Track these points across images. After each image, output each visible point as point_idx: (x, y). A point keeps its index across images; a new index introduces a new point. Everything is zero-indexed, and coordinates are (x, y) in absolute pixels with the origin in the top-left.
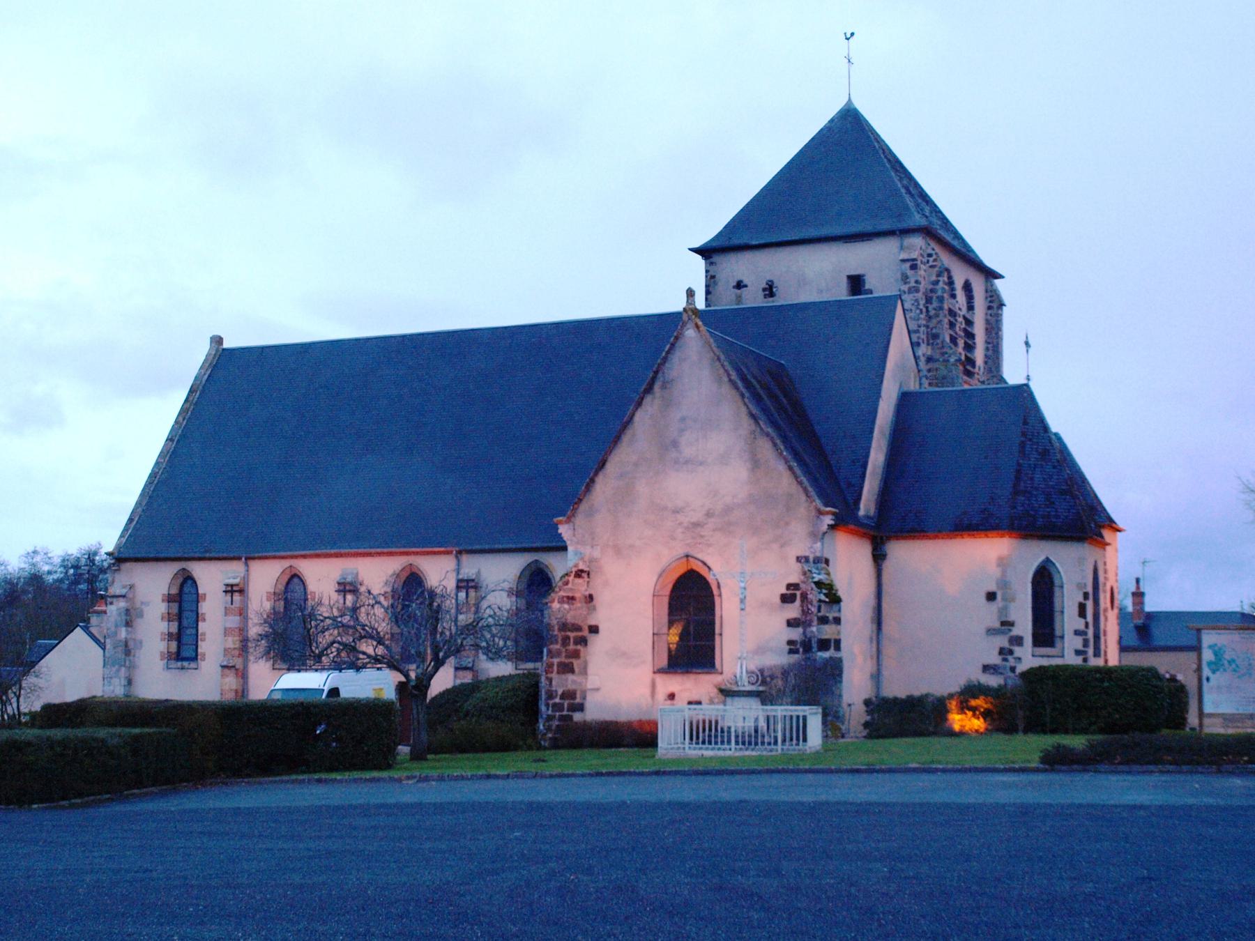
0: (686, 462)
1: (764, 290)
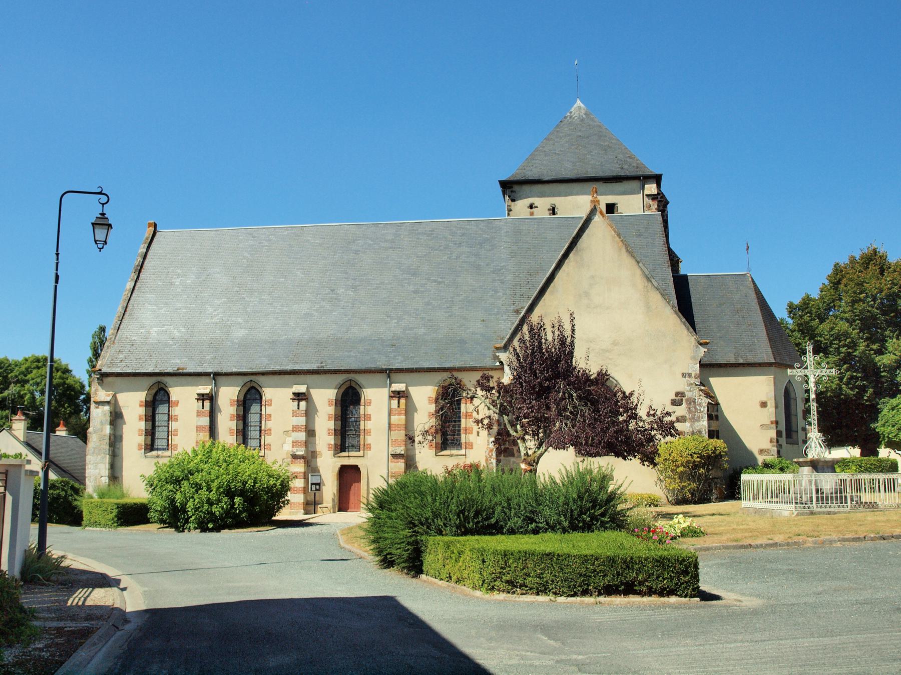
1: (549, 210)
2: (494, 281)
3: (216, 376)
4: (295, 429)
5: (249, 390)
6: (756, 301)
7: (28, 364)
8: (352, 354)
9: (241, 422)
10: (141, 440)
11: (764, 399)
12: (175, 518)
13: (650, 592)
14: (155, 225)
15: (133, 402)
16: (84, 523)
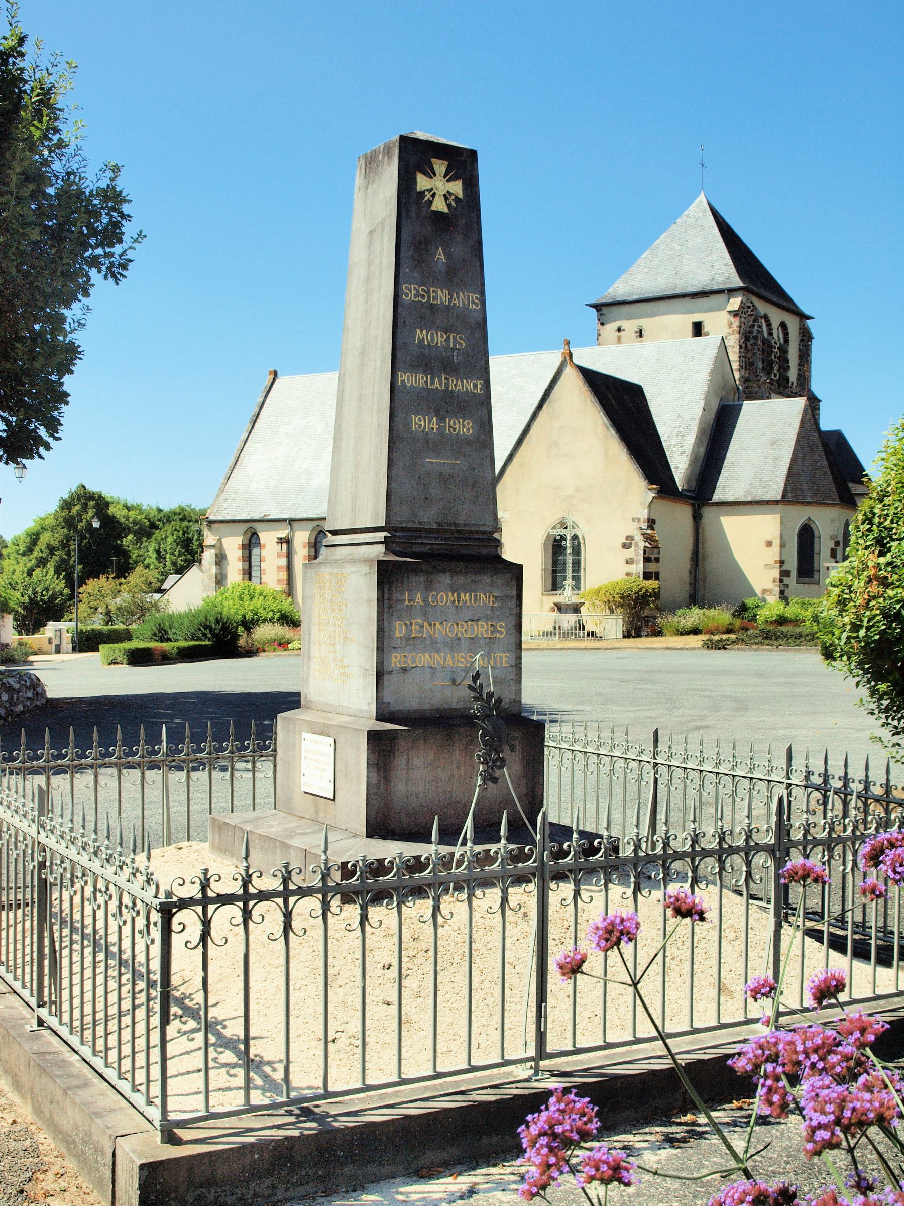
1: (636, 332)
11: (769, 538)
14: (275, 374)
15: (233, 545)
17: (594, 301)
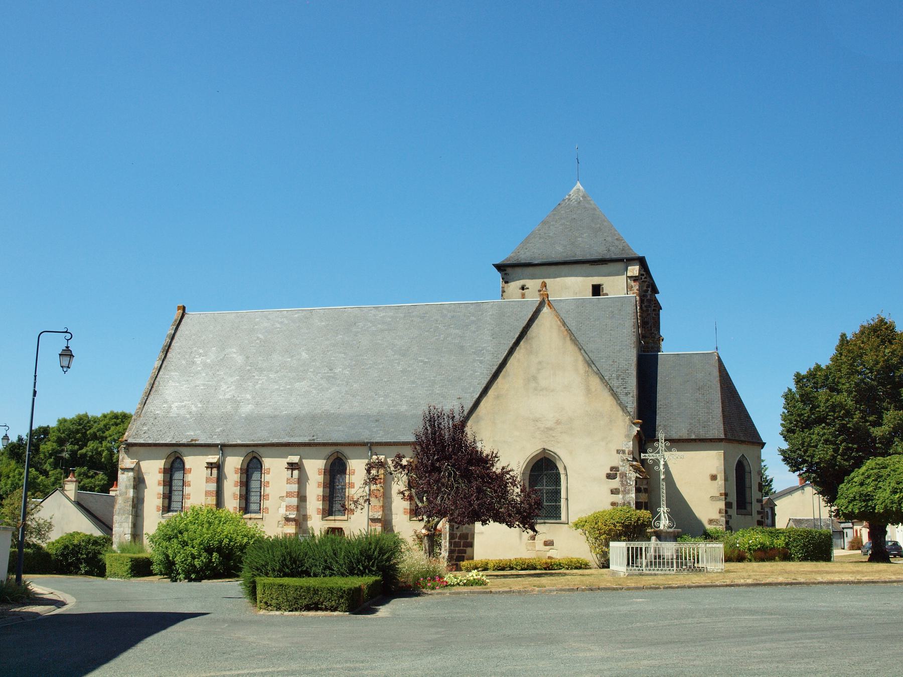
0: (542, 390)
2: (474, 361)
3: (223, 448)
4: (289, 494)
5: (251, 460)
6: (718, 379)
7: (107, 421)
8: (341, 428)
9: (244, 488)
10: (159, 502)
11: (714, 473)
12: (169, 570)
13: (326, 609)
14: (184, 308)
15: (153, 470)
16: (107, 574)
17: (497, 262)
